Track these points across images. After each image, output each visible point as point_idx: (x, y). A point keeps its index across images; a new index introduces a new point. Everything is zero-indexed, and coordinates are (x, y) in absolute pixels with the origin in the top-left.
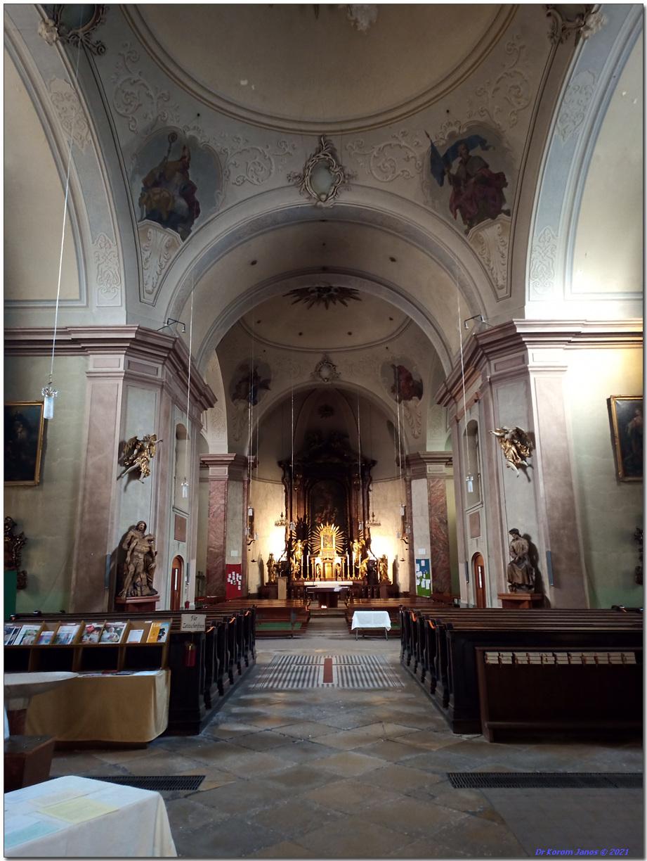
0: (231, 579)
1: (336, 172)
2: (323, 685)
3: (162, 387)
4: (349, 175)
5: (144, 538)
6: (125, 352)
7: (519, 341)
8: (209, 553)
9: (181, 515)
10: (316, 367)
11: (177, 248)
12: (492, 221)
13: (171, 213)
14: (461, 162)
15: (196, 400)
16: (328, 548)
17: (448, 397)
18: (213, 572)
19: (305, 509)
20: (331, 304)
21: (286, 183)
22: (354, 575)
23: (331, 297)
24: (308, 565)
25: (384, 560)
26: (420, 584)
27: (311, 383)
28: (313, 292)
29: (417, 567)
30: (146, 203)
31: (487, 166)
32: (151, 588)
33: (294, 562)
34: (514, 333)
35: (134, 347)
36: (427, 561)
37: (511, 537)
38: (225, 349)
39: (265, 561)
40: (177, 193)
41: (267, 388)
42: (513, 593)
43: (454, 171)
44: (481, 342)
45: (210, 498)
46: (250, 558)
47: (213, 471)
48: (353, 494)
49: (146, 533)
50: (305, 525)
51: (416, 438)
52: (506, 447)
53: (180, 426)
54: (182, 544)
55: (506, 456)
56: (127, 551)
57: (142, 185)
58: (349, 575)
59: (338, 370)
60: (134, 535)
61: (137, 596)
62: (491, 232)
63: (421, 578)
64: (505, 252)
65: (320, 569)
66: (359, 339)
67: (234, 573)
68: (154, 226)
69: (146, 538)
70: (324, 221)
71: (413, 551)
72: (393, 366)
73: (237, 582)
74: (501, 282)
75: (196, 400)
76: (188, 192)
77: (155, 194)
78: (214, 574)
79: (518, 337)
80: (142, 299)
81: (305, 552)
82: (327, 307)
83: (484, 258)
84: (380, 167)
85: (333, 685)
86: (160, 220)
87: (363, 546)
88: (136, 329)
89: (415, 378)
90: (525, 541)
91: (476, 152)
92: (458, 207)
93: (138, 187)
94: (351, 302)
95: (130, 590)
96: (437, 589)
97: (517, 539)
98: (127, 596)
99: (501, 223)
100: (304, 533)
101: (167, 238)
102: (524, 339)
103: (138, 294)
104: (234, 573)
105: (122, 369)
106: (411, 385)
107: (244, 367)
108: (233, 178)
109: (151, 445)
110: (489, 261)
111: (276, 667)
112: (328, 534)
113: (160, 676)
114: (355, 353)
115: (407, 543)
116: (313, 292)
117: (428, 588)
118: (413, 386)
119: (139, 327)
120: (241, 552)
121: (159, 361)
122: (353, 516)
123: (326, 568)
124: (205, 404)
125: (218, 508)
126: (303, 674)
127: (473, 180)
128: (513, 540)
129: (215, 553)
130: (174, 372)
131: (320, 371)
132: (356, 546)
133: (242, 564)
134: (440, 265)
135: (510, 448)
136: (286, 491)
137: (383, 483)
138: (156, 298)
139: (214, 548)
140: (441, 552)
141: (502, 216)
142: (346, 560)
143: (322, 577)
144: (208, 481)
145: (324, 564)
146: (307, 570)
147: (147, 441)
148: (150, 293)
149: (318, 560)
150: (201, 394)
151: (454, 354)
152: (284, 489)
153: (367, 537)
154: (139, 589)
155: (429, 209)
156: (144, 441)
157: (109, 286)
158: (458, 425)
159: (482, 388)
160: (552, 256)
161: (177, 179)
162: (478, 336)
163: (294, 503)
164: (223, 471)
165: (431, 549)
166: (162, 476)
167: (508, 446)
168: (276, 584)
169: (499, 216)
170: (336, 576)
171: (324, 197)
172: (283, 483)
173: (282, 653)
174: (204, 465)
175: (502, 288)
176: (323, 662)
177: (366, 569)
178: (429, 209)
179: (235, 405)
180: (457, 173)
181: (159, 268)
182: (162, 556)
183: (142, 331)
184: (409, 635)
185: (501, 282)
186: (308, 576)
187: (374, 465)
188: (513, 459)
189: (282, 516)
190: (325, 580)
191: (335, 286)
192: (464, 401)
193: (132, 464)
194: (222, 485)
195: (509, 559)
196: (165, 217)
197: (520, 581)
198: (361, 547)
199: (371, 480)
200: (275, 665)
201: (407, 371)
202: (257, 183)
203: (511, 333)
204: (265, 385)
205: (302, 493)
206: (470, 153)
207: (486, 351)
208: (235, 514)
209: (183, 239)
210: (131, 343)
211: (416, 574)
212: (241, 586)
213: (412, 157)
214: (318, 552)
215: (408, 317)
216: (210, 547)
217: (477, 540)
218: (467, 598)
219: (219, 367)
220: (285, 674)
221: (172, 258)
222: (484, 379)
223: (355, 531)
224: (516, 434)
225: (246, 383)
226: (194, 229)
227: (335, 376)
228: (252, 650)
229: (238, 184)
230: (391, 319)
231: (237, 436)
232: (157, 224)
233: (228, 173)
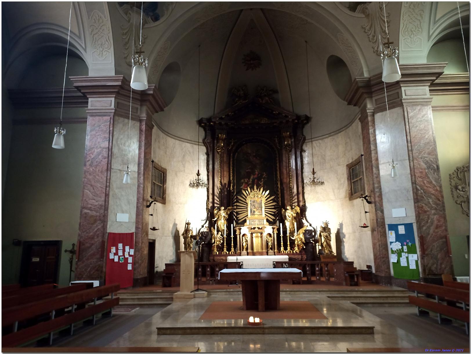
0: (116, 254)
6: (114, 96)
8: (84, 216)
16: (256, 216)
18: (88, 245)
22: (289, 248)
24: (232, 236)
25: (326, 229)
26: (399, 261)
29: (391, 236)
33: (215, 232)
36: (408, 227)
39: (182, 230)
48: (284, 156)
50: (229, 191)
58: (282, 248)
63: (399, 253)
65: (247, 241)
67: (120, 246)
71: (382, 211)
73: (126, 259)
81: (229, 220)
87: (297, 213)
96: (430, 270)
100: (228, 200)
104: (120, 246)
105: (113, 107)
112: (256, 199)
117: (413, 266)
120: (134, 216)
122: (285, 181)
123: (254, 239)
125: (99, 154)
132: (289, 213)
133: (136, 233)
136: (207, 154)
137: (320, 141)
139: (90, 209)
140: (433, 212)
142: (279, 230)
143: (249, 251)
145: (252, 234)
146: (232, 242)
149: (245, 230)
152: (205, 151)
153: (301, 204)
160: (420, 18)
170: (267, 249)
172: (204, 143)
177: (303, 240)
186: (233, 249)
187: (308, 122)
190: (254, 254)
194: (106, 121)
198: (295, 215)
199: (305, 139)
205: (225, 156)
211: (390, 247)
212: (133, 264)
214: (245, 221)
216: (83, 208)
223: (286, 197)
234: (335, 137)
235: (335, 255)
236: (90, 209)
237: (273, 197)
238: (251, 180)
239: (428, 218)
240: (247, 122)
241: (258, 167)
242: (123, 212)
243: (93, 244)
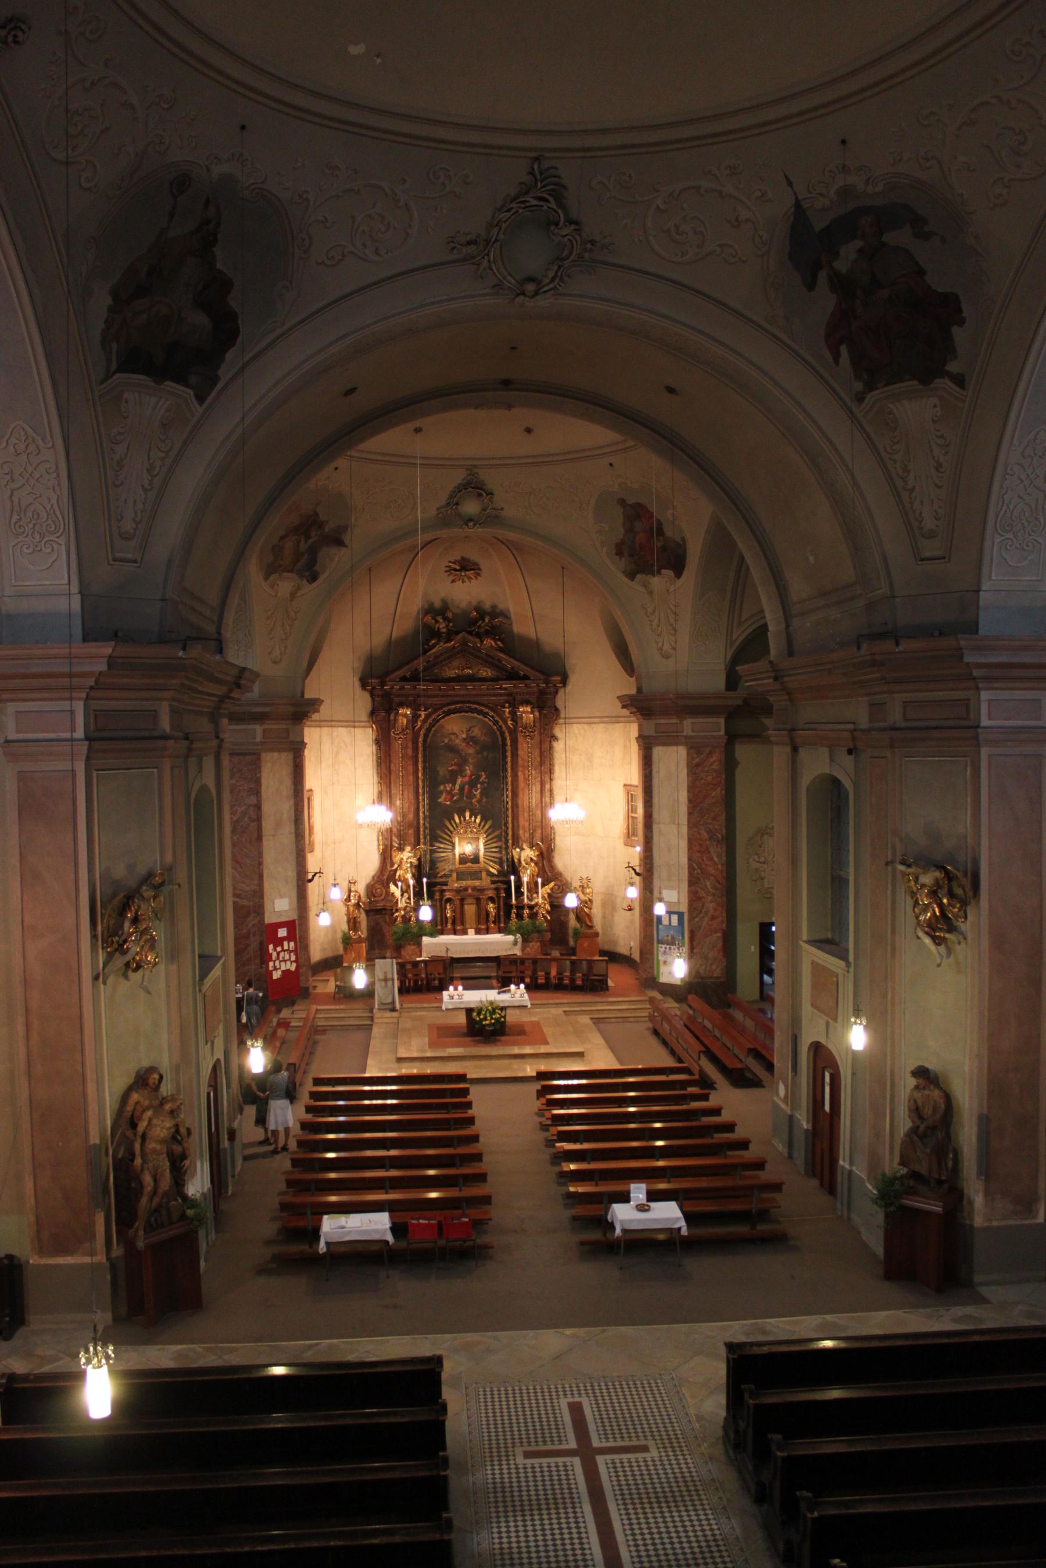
4: (593, 242)
14: (860, 251)
31: (922, 273)
33: (395, 890)
41: (340, 543)
43: (842, 265)
51: (667, 657)
57: (109, 301)
62: (916, 410)
72: (622, 502)
74: (929, 523)
76: (214, 296)
83: (895, 461)
84: (668, 231)
89: (669, 532)
91: (901, 238)
93: (101, 302)
115: (638, 874)
136: (377, 742)
137: (586, 726)
140: (710, 898)
141: (945, 383)
157: (37, 537)
165: (690, 892)
169: (937, 380)
175: (931, 535)
179: (272, 587)
185: (929, 523)
206: (885, 238)
208: (278, 824)
209: (201, 399)
213: (747, 220)
226: (225, 372)
229: (329, 263)
234: (610, 726)
237: (497, 833)
238: (457, 787)
239: (703, 906)
242: (281, 897)
243: (248, 945)
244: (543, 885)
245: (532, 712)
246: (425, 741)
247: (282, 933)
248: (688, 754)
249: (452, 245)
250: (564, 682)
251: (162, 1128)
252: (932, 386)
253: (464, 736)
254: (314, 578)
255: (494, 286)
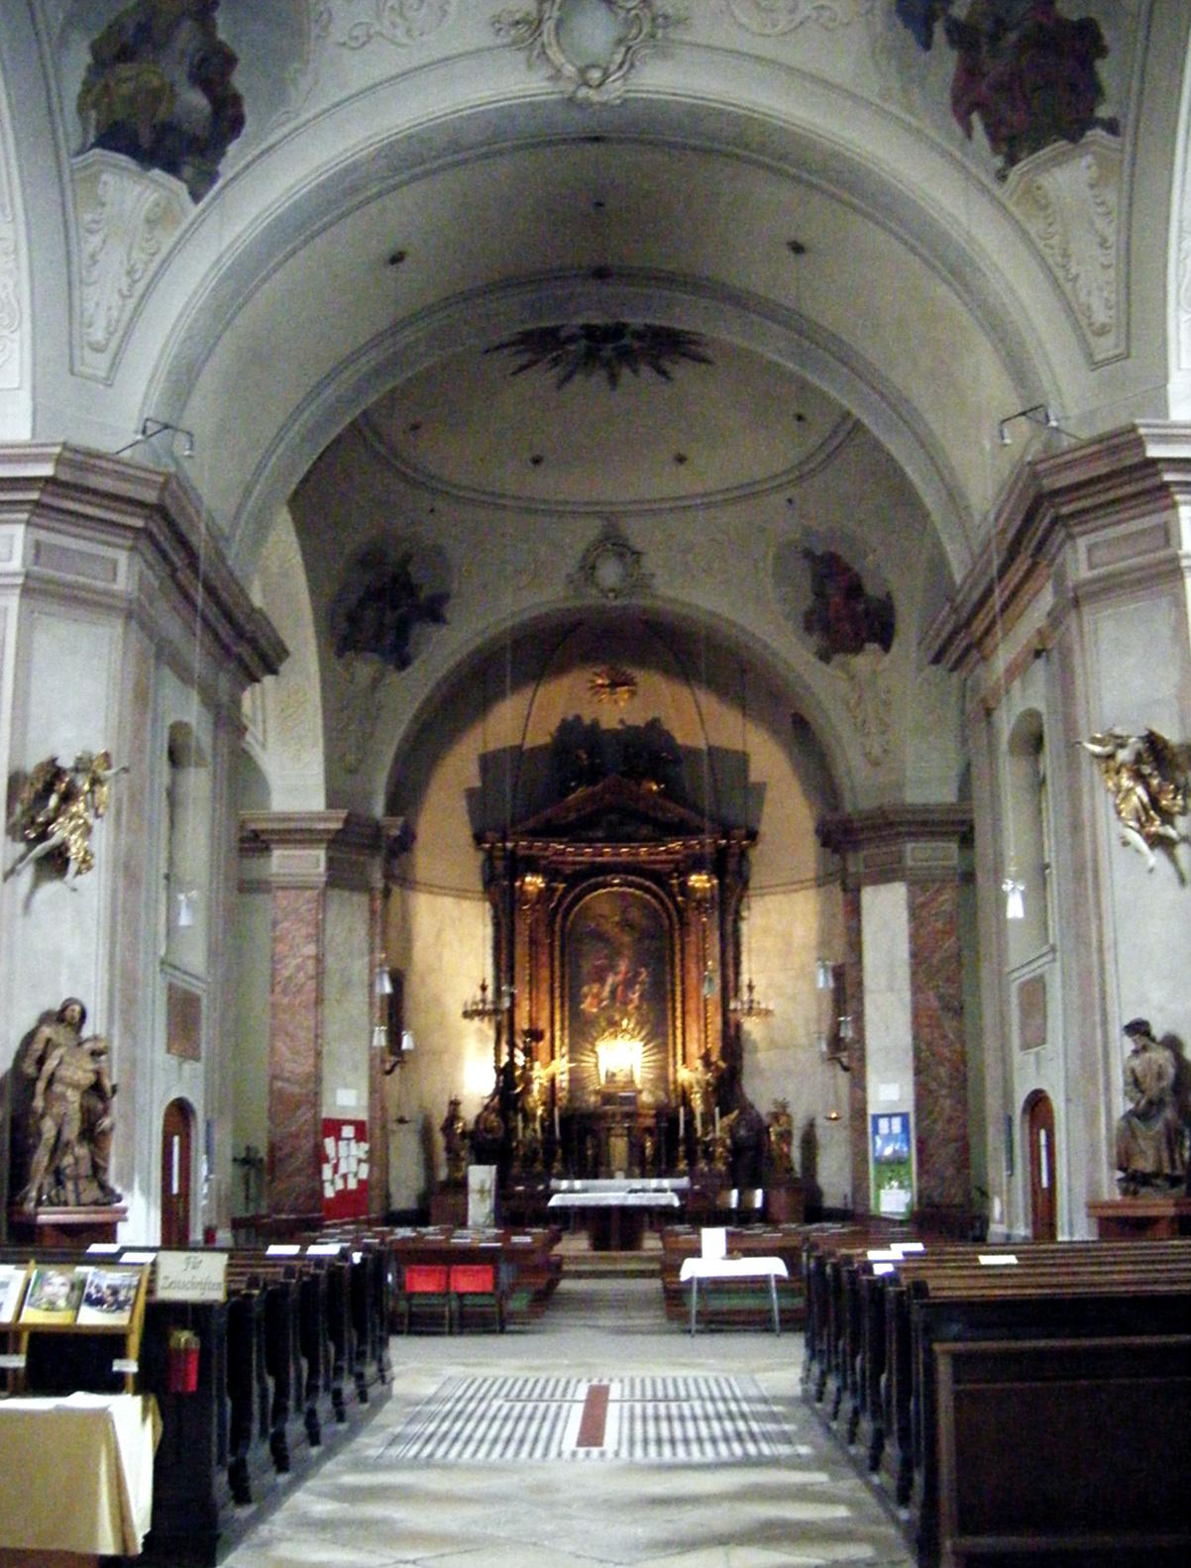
1: (629, 10)
2: (574, 1454)
3: (129, 616)
4: (666, 17)
5: (80, 1044)
6: (25, 516)
7: (1155, 481)
9: (182, 982)
10: (584, 558)
11: (179, 223)
12: (1070, 146)
13: (166, 129)
15: (226, 649)
17: (961, 642)
18: (287, 1150)
19: (552, 972)
20: (626, 373)
21: (487, 39)
23: (626, 356)
27: (569, 604)
28: (571, 339)
30: (95, 105)
32: (103, 1187)
34: (1136, 460)
35: (48, 500)
37: (1129, 1044)
38: (313, 502)
39: (439, 1121)
40: (179, 74)
42: (1129, 1200)
44: (1049, 483)
45: (275, 940)
46: (393, 1114)
47: (282, 862)
49: (87, 1032)
52: (1118, 787)
53: (179, 730)
54: (187, 1067)
55: (1119, 813)
56: (34, 1081)
57: (88, 59)
59: (649, 564)
60: (54, 1036)
61: (66, 1204)
62: (1068, 177)
64: (1110, 232)
66: (711, 471)
68: (115, 166)
69: (88, 1046)
70: (597, 139)
72: (808, 554)
74: (1101, 317)
75: (226, 649)
76: (214, 70)
77: (120, 81)
78: (290, 1156)
79: (1150, 470)
80: (78, 368)
82: (613, 380)
83: (1052, 248)
85: (602, 1454)
86: (133, 150)
88: (57, 450)
89: (871, 589)
90: (1167, 1054)
92: (977, 105)
93: (78, 60)
94: (683, 371)
95: (46, 1188)
96: (929, 1197)
97: (1145, 1049)
98: (39, 1203)
99: (1094, 153)
101: (152, 196)
102: (1168, 477)
103: (68, 353)
106: (861, 607)
107: (369, 559)
108: (338, 32)
109: (96, 781)
110: (1065, 255)
111: (448, 1406)
113: (131, 1427)
114: (695, 513)
116: (571, 339)
118: (867, 613)
119: (59, 461)
121: (120, 541)
124: (253, 662)
125: (299, 968)
126: (522, 1425)
127: (1013, 36)
128: (1136, 1052)
129: (292, 1095)
130: (164, 572)
131: (593, 568)
134: (933, 268)
135: (1130, 790)
138: (114, 365)
139: (288, 1080)
140: (944, 1092)
141: (1097, 134)
144: (268, 891)
147: (86, 770)
148: (98, 349)
150: (240, 634)
151: (977, 518)
154: (70, 1186)
155: (895, 110)
156: (76, 770)
158: (989, 724)
159: (1055, 618)
161: (186, 37)
162: (1040, 467)
163: (521, 952)
164: (313, 862)
166: (128, 871)
167: (1126, 782)
168: (460, 1186)
171: (595, 75)
173: (471, 1370)
174: (255, 842)
175: (1102, 331)
176: (582, 1393)
177: (728, 1141)
178: (895, 110)
180: (970, 15)
181: (125, 281)
182: (131, 1098)
183: (76, 458)
184: (824, 1322)
185: (1101, 317)
188: (1138, 820)
189: (484, 988)
191: (636, 321)
192: (1004, 656)
193: (43, 836)
195: (1122, 1105)
196: (146, 139)
197: (1145, 1164)
200: (446, 1400)
201: (848, 569)
202: (404, 40)
203: (1130, 459)
204: (434, 611)
207: (1065, 510)
208: (347, 985)
209: (196, 197)
210: (43, 491)
215: (847, 415)
217: (1037, 1054)
218: (1007, 1213)
219: (297, 560)
220: (471, 1425)
221: (164, 251)
222: (1059, 590)
224: (1148, 749)
225: (380, 607)
226: (227, 167)
227: (640, 584)
228: (380, 1360)
229: (354, 44)
230: (800, 418)
231: (351, 758)
232: (122, 159)
233: (325, 16)
235: (799, 1176)
236: (288, 1080)
239: (936, 1102)
240: (600, 834)
241: (626, 952)
244: (722, 1115)
245: (709, 881)
246: (563, 927)
247: (348, 1131)
248: (909, 891)
249: (497, 26)
250: (753, 836)
251: (80, 1072)
252: (1083, 141)
253: (617, 919)
254: (403, 663)
255: (550, 78)
